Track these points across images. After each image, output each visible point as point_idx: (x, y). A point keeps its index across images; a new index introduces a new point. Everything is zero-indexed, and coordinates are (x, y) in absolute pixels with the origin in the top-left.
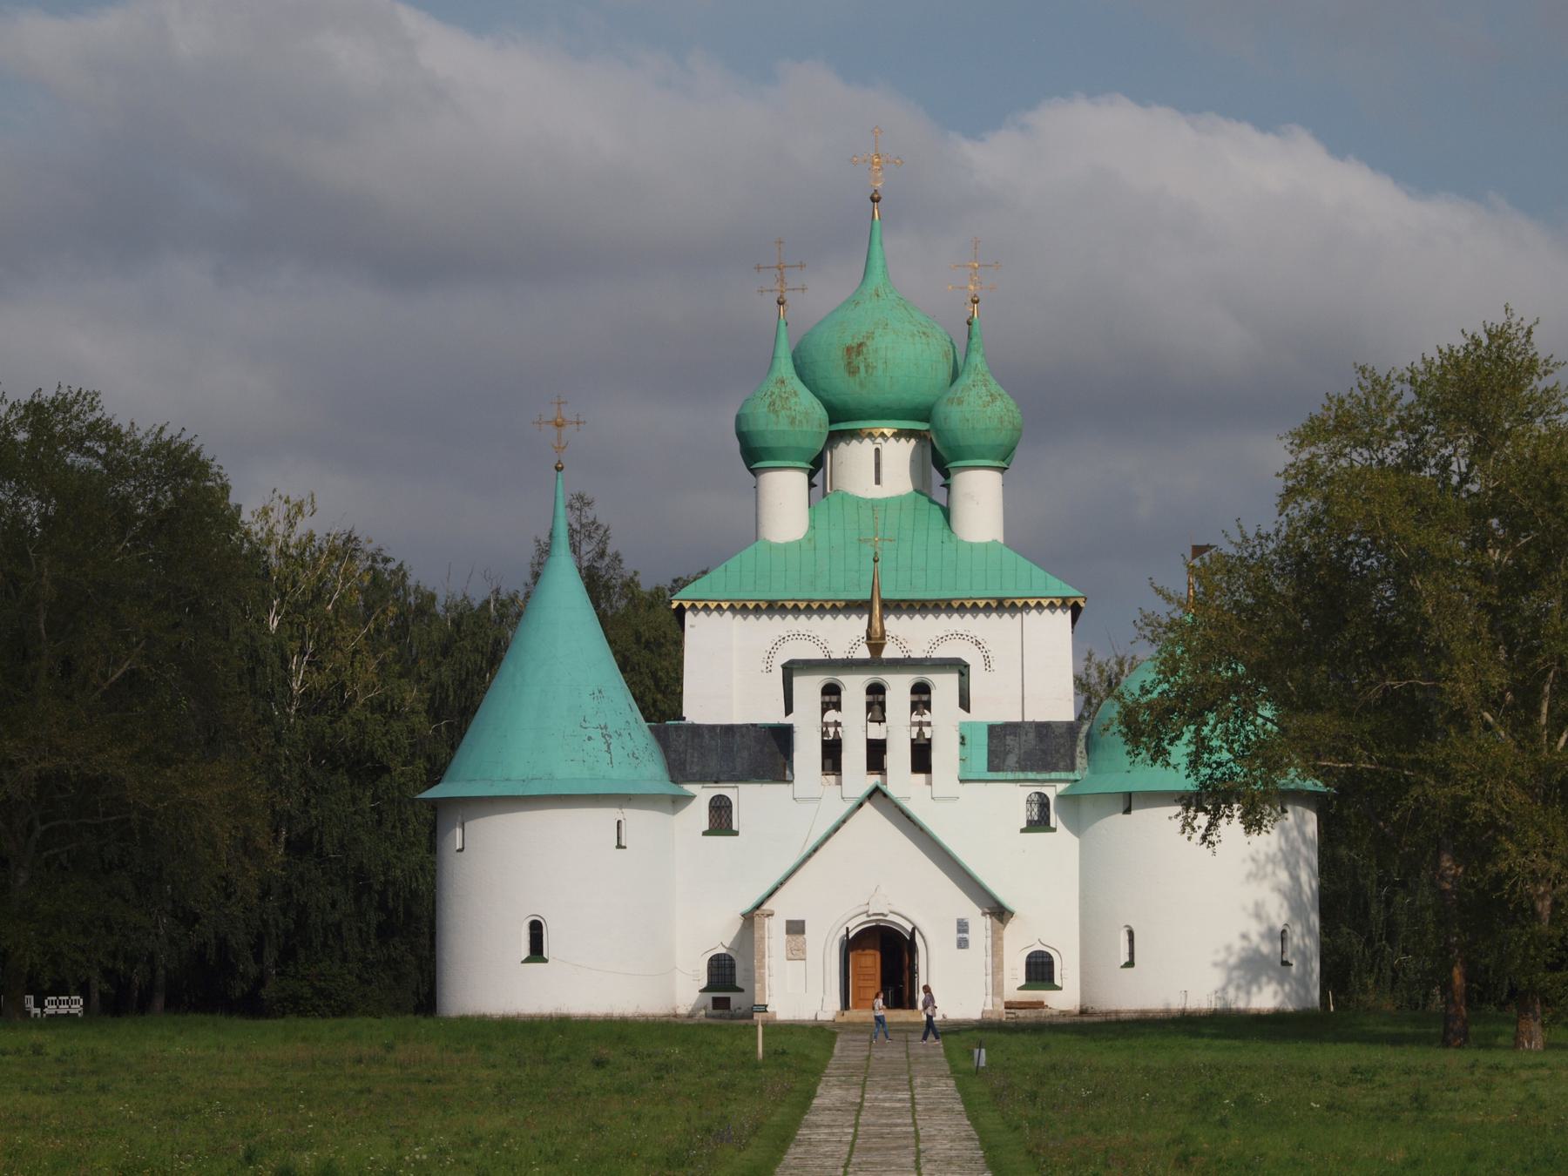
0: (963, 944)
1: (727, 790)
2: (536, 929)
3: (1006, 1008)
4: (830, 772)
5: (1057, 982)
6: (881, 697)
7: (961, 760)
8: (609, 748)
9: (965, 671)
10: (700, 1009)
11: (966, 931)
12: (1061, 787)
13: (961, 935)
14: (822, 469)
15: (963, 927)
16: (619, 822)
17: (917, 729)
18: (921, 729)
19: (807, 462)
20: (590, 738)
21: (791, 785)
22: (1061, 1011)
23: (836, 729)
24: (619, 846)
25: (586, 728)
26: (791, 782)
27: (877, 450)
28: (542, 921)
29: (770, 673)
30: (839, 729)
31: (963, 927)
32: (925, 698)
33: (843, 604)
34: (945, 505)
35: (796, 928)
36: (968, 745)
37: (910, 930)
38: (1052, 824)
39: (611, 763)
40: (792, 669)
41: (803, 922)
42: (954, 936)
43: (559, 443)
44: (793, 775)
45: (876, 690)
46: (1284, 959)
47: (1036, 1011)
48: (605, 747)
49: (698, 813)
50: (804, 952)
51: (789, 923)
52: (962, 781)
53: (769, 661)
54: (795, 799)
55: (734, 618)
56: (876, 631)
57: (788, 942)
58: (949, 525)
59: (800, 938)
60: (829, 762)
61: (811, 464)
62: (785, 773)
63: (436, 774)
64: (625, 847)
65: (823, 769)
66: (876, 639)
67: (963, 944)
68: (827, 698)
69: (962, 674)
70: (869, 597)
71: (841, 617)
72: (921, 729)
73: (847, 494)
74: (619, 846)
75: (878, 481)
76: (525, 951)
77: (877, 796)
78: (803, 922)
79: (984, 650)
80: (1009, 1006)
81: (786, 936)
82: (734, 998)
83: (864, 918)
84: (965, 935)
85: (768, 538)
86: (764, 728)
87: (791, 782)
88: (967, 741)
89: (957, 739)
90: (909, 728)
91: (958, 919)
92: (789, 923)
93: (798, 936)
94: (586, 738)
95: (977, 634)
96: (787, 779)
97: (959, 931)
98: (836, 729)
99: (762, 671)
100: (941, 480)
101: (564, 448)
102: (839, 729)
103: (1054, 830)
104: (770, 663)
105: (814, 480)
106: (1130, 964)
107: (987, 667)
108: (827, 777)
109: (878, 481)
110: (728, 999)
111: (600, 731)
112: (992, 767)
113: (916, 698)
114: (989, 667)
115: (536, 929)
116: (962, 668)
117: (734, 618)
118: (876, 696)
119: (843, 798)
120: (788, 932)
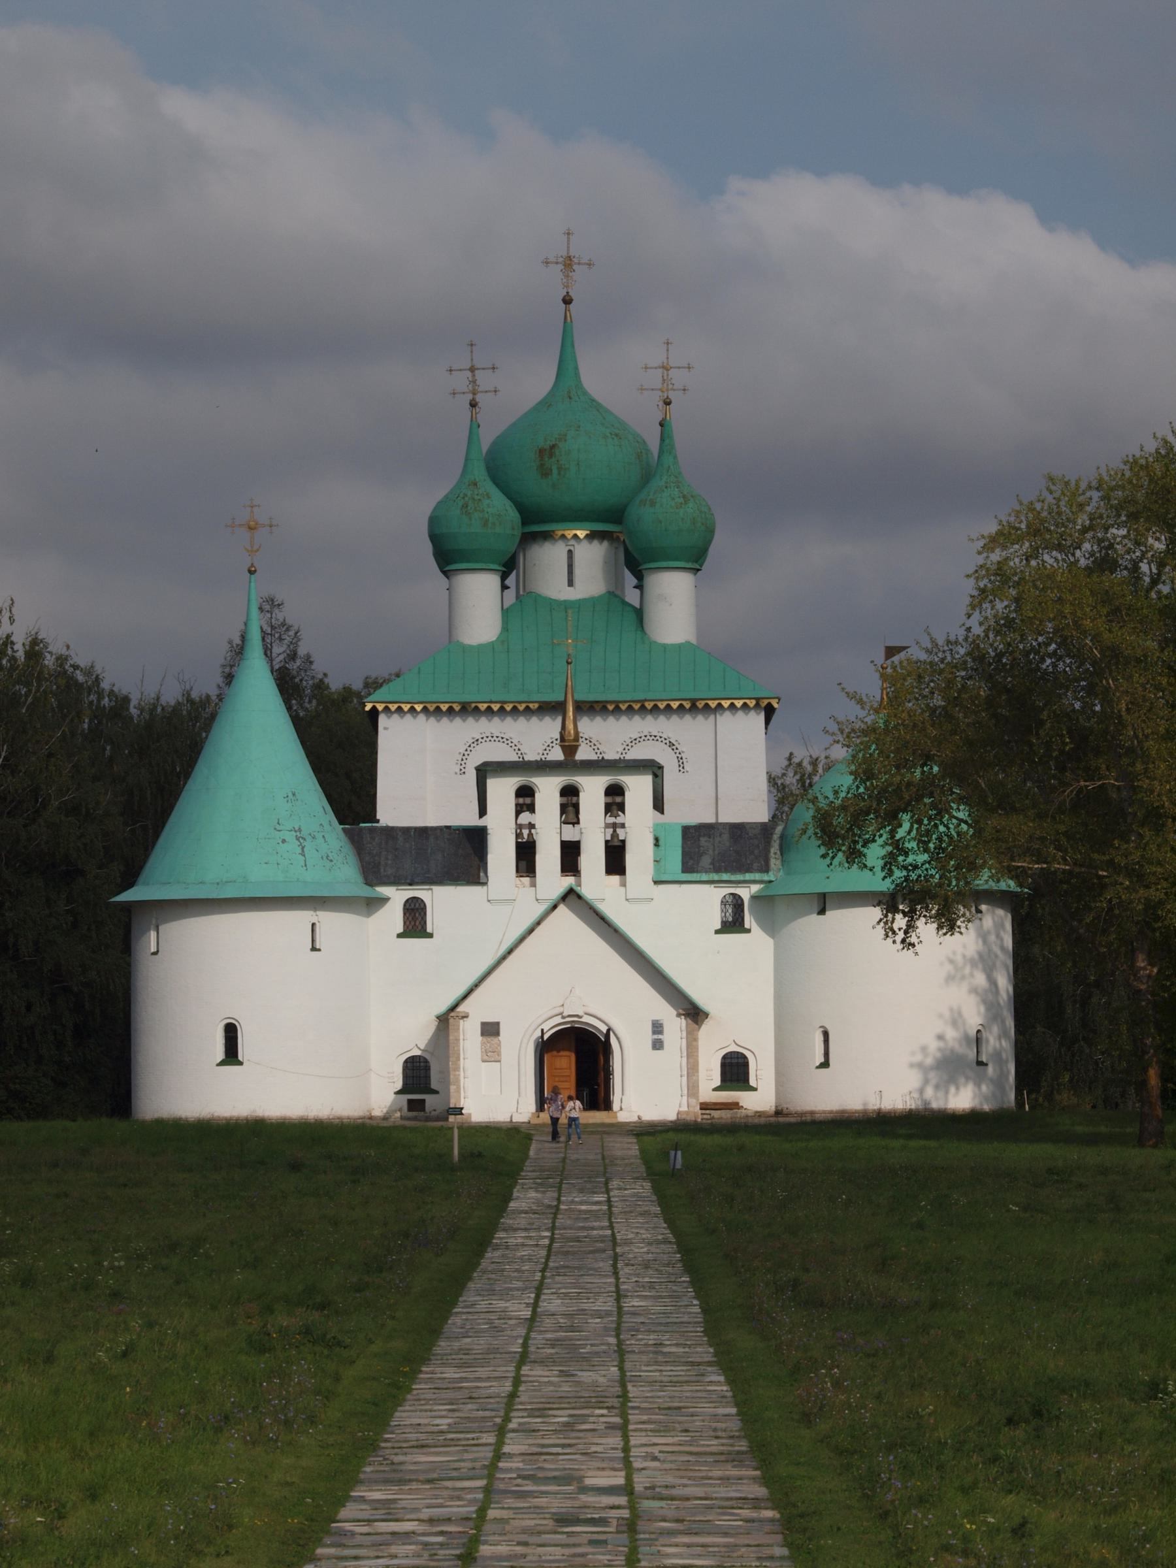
0: (658, 1045)
1: (421, 893)
2: (231, 1031)
3: (701, 1109)
4: (524, 874)
5: (752, 1082)
6: (575, 799)
7: (655, 861)
8: (303, 848)
9: (659, 773)
10: (396, 1111)
11: (661, 1032)
12: (755, 888)
13: (656, 1037)
14: (514, 572)
15: (657, 1028)
16: (313, 925)
17: (610, 831)
18: (615, 831)
19: (499, 565)
20: (284, 841)
21: (485, 887)
22: (756, 1112)
23: (530, 831)
24: (314, 949)
25: (279, 831)
26: (485, 884)
27: (570, 552)
28: (233, 1022)
29: (463, 776)
30: (533, 831)
31: (657, 1028)
32: (618, 799)
33: (536, 705)
34: (638, 606)
35: (490, 1030)
36: (662, 848)
37: (605, 1032)
38: (747, 926)
39: (306, 866)
40: (486, 771)
41: (498, 1024)
42: (649, 1037)
43: (252, 547)
44: (487, 876)
45: (570, 793)
46: (980, 1060)
47: (732, 1111)
48: (299, 850)
49: (392, 915)
50: (499, 1054)
51: (484, 1024)
52: (656, 882)
53: (463, 763)
54: (489, 901)
55: (427, 720)
56: (569, 733)
57: (483, 1044)
58: (642, 627)
59: (494, 1040)
60: (523, 864)
61: (504, 566)
62: (479, 875)
63: (130, 878)
64: (319, 950)
65: (517, 871)
66: (570, 741)
67: (658, 1045)
68: (521, 800)
69: (655, 776)
70: (563, 699)
71: (534, 719)
72: (615, 831)
73: (540, 596)
74: (314, 949)
75: (571, 583)
76: (220, 1053)
77: (572, 897)
78: (498, 1024)
79: (678, 751)
80: (704, 1106)
81: (481, 1038)
82: (429, 1099)
83: (559, 1020)
84: (660, 1037)
85: (461, 639)
86: (458, 830)
87: (485, 884)
88: (661, 842)
89: (651, 841)
90: (603, 830)
91: (653, 1021)
92: (484, 1024)
93: (492, 1038)
94: (280, 841)
95: (670, 735)
96: (481, 881)
97: (654, 1033)
98: (530, 831)
99: (456, 773)
100: (635, 581)
101: (258, 550)
102: (533, 831)
103: (749, 931)
104: (464, 765)
105: (507, 582)
106: (825, 1064)
107: (681, 768)
108: (521, 879)
109: (571, 583)
110: (423, 1101)
111: (295, 834)
112: (686, 869)
113: (610, 800)
114: (683, 768)
115: (231, 1031)
116: (656, 770)
117: (427, 720)
118: (570, 798)
119: (537, 900)
120: (483, 1034)
